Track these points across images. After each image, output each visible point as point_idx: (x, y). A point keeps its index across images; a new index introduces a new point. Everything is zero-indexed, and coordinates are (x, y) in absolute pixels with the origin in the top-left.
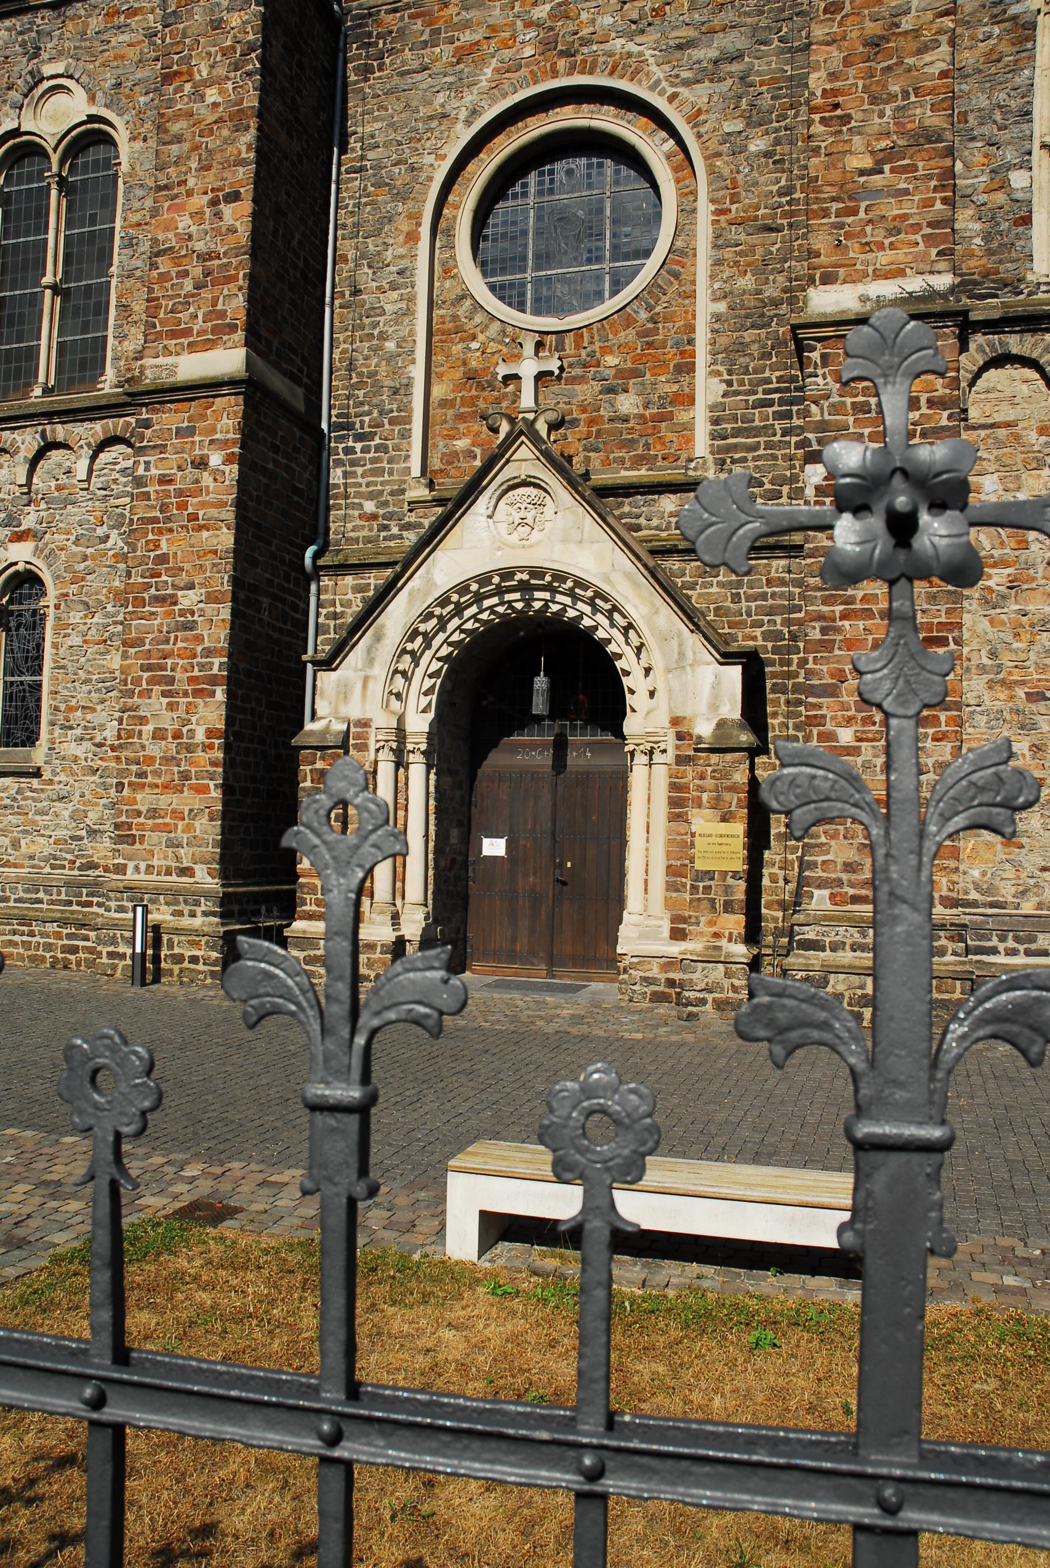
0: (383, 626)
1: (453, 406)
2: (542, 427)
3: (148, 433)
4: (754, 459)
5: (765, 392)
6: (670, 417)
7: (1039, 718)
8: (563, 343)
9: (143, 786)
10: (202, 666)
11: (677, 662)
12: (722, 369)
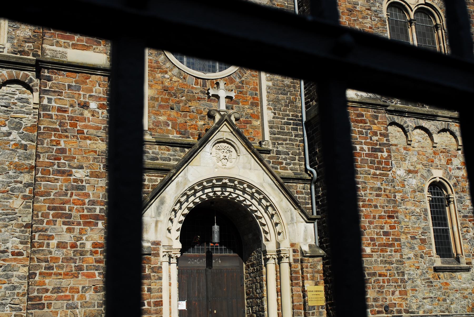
0: (164, 197)
1: (158, 101)
2: (233, 119)
3: (49, 83)
4: (286, 144)
5: (288, 119)
6: (250, 123)
7: (415, 245)
8: (206, 84)
9: (50, 275)
10: (89, 210)
11: (291, 221)
12: (272, 107)
